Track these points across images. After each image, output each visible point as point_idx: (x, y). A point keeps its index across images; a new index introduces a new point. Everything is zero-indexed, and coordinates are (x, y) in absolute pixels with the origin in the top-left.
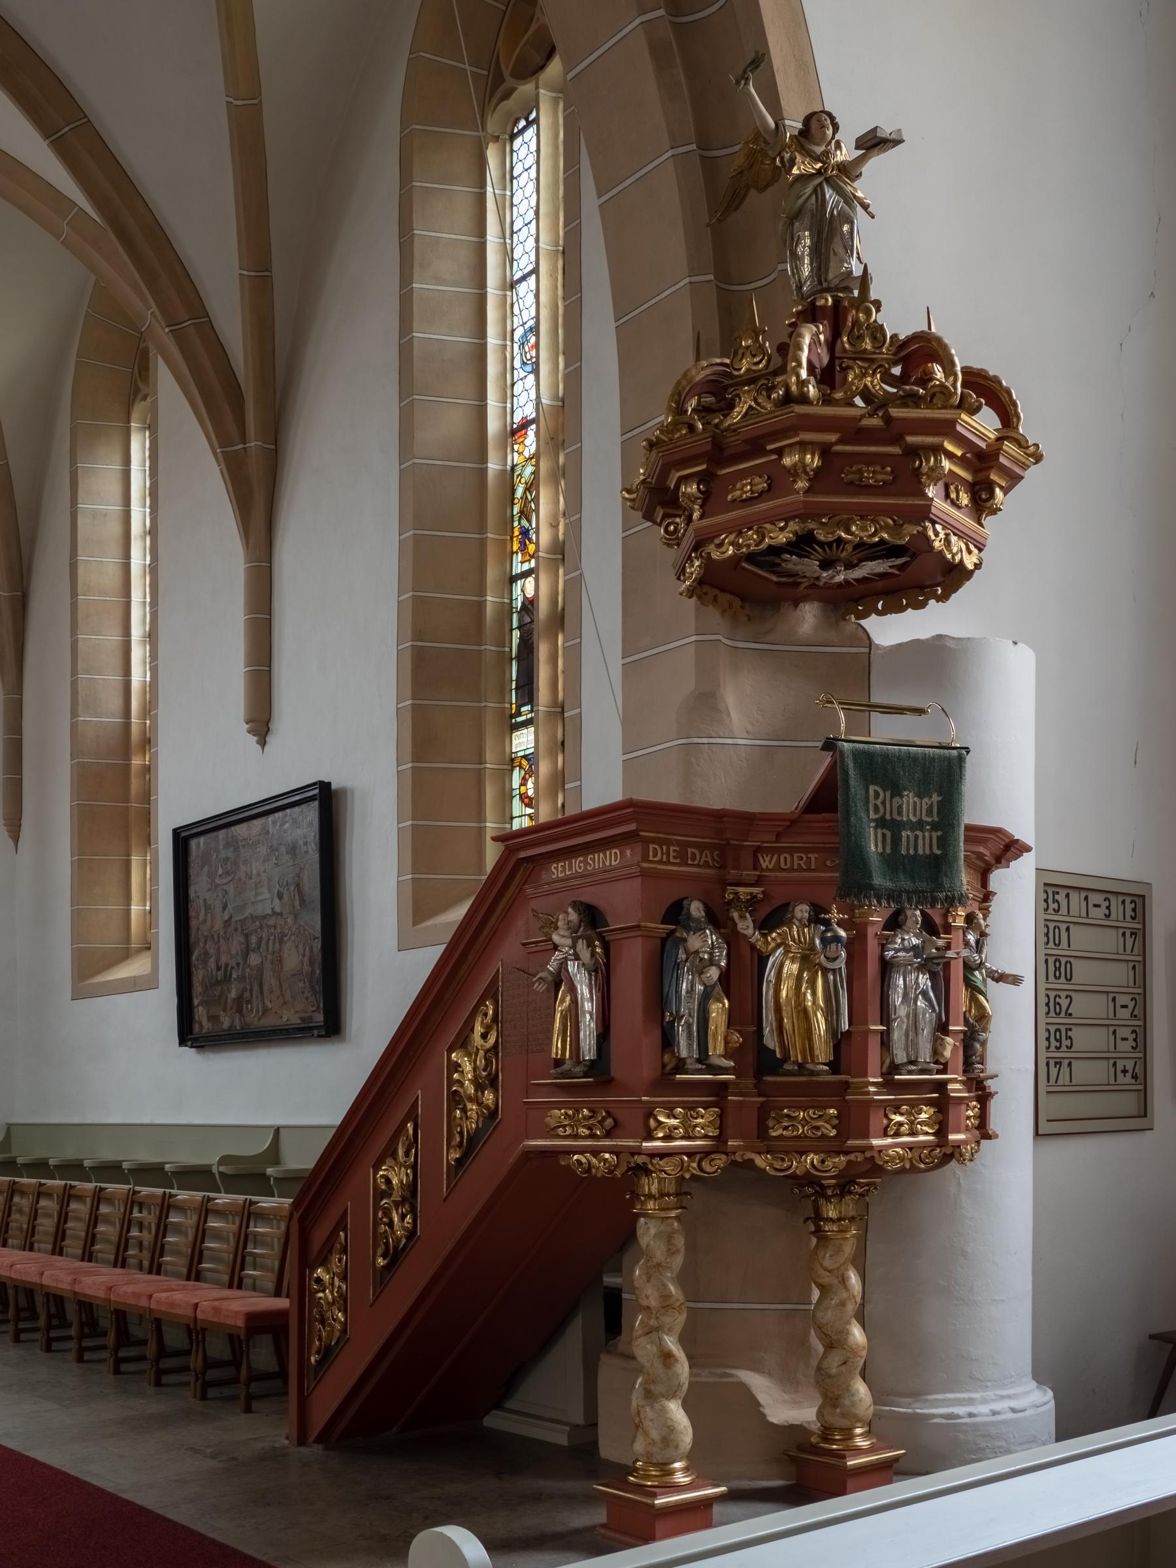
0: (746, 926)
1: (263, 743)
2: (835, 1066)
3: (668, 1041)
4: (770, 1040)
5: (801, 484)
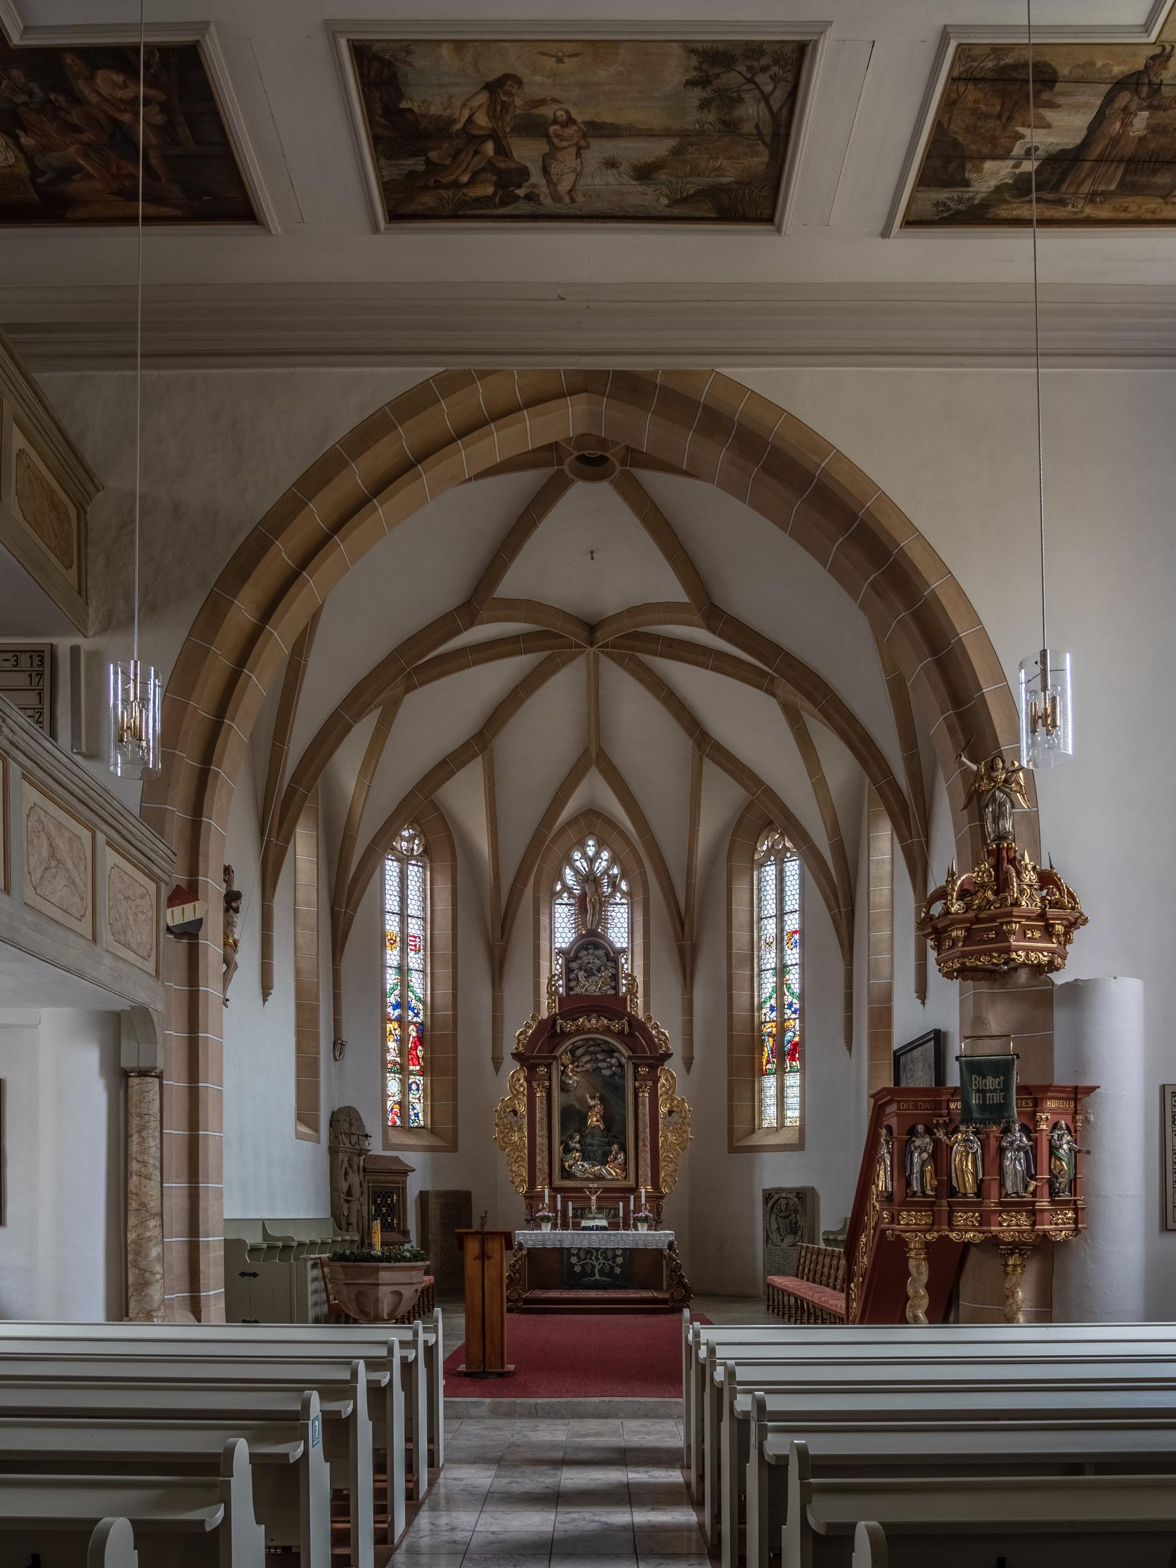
0: (941, 1135)
1: (923, 1003)
2: (978, 1194)
3: (909, 1184)
4: (954, 1183)
5: (960, 944)
